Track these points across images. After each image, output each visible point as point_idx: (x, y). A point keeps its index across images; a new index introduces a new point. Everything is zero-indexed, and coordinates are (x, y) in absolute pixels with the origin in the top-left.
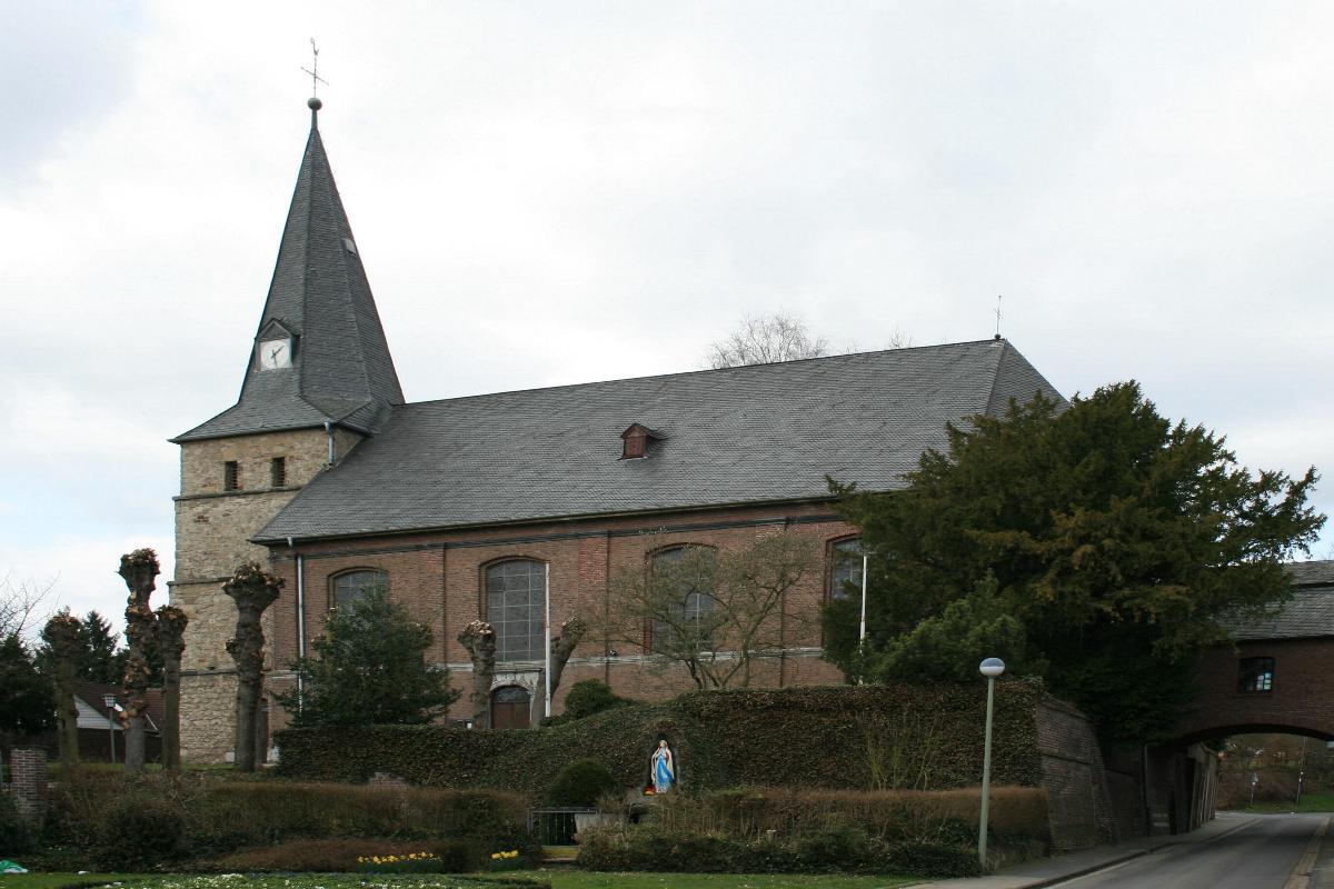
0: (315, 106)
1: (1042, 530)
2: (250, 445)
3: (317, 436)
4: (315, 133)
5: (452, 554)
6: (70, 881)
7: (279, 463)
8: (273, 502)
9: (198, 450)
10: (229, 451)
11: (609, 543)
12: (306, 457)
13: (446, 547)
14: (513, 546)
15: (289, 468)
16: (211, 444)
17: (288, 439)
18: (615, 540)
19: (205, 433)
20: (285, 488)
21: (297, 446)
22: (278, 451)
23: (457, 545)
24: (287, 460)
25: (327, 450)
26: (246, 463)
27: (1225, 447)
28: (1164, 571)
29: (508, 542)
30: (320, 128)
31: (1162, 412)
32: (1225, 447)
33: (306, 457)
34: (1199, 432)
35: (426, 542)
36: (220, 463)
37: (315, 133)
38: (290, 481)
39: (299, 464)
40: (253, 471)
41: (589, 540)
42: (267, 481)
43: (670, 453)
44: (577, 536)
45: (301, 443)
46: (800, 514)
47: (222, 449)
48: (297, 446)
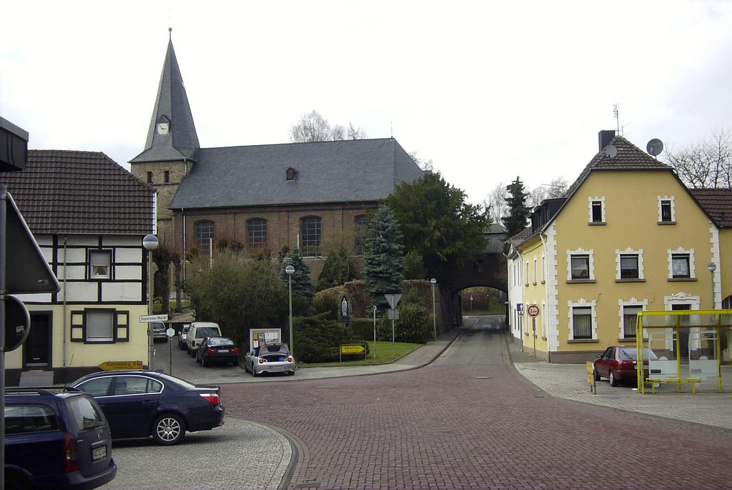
0: (170, 30)
1: (425, 223)
2: (156, 165)
3: (181, 164)
4: (170, 40)
5: (237, 216)
6: (370, 370)
7: (167, 173)
8: (165, 189)
9: (137, 166)
10: (149, 168)
11: (288, 215)
12: (177, 172)
13: (235, 213)
14: (257, 214)
15: (170, 175)
16: (142, 164)
17: (170, 164)
18: (290, 213)
19: (140, 160)
20: (169, 183)
21: (174, 167)
22: (167, 168)
23: (238, 213)
24: (170, 172)
25: (184, 169)
26: (155, 173)
27: (464, 193)
28: (457, 236)
29: (255, 212)
30: (171, 39)
31: (447, 181)
32: (464, 193)
33: (177, 172)
34: (438, 176)
35: (228, 212)
36: (145, 172)
37: (170, 40)
38: (171, 181)
39: (174, 174)
40: (157, 176)
41: (282, 213)
42: (162, 180)
43: (302, 180)
44: (278, 212)
45: (175, 166)
46: (346, 207)
47: (147, 167)
48: (174, 167)
